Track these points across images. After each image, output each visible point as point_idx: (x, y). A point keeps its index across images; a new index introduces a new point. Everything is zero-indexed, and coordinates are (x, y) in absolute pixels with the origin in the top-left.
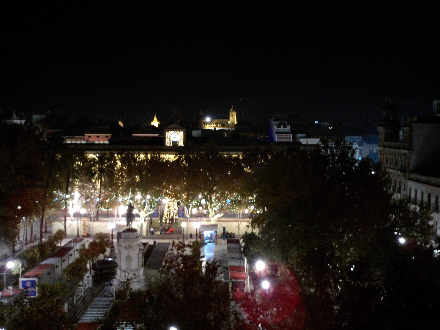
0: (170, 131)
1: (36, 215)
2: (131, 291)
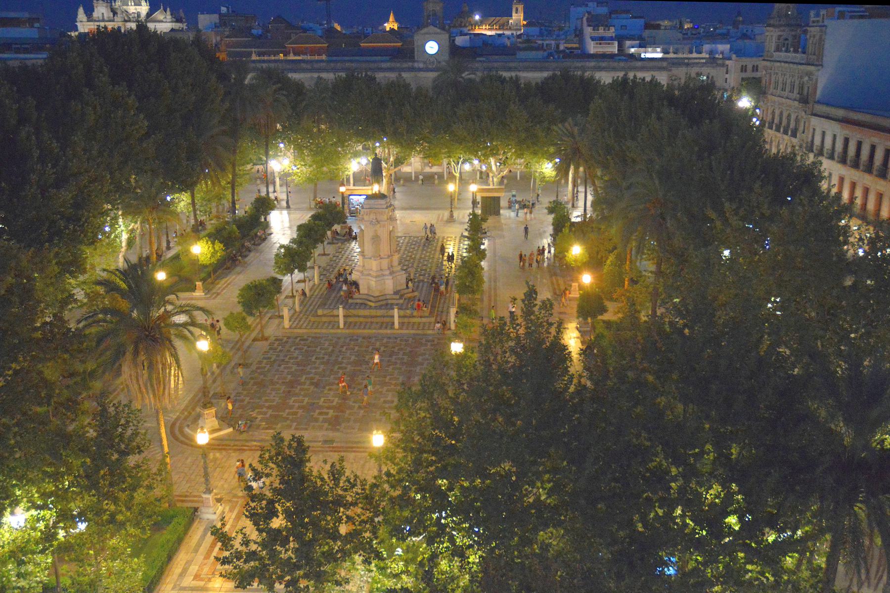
1: (588, 187)
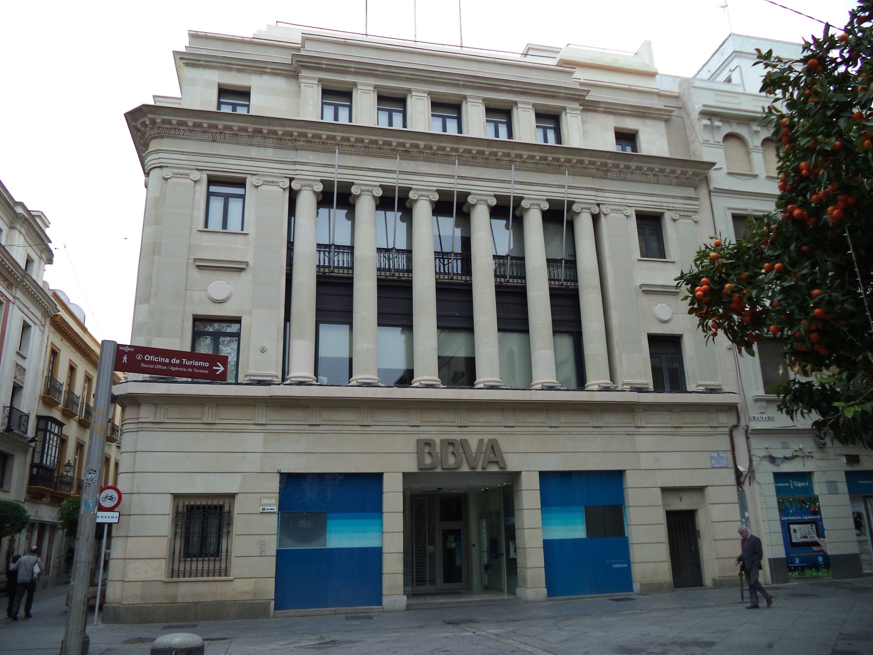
0: (546, 589)
2: (737, 122)
